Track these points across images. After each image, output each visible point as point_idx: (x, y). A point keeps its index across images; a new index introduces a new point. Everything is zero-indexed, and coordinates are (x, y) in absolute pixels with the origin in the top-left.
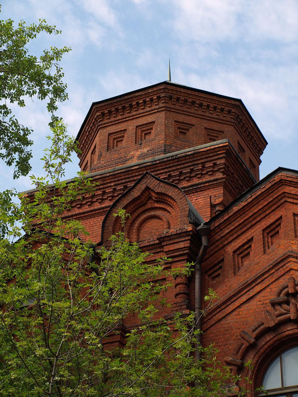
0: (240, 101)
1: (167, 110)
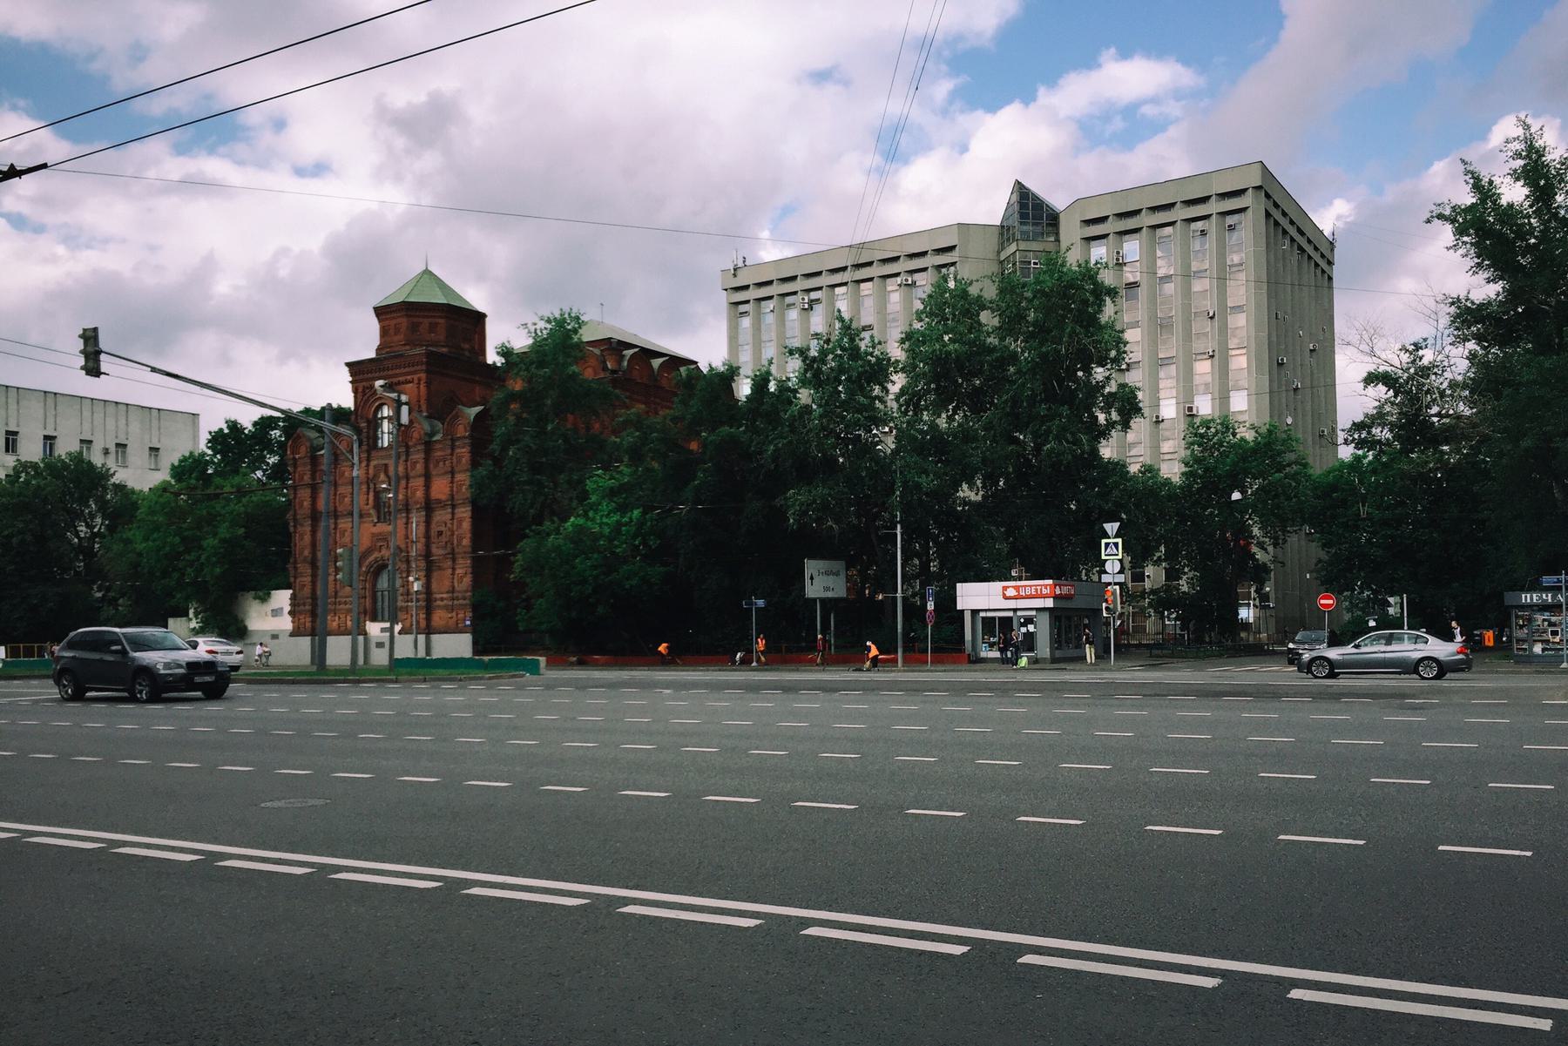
1: (407, 316)
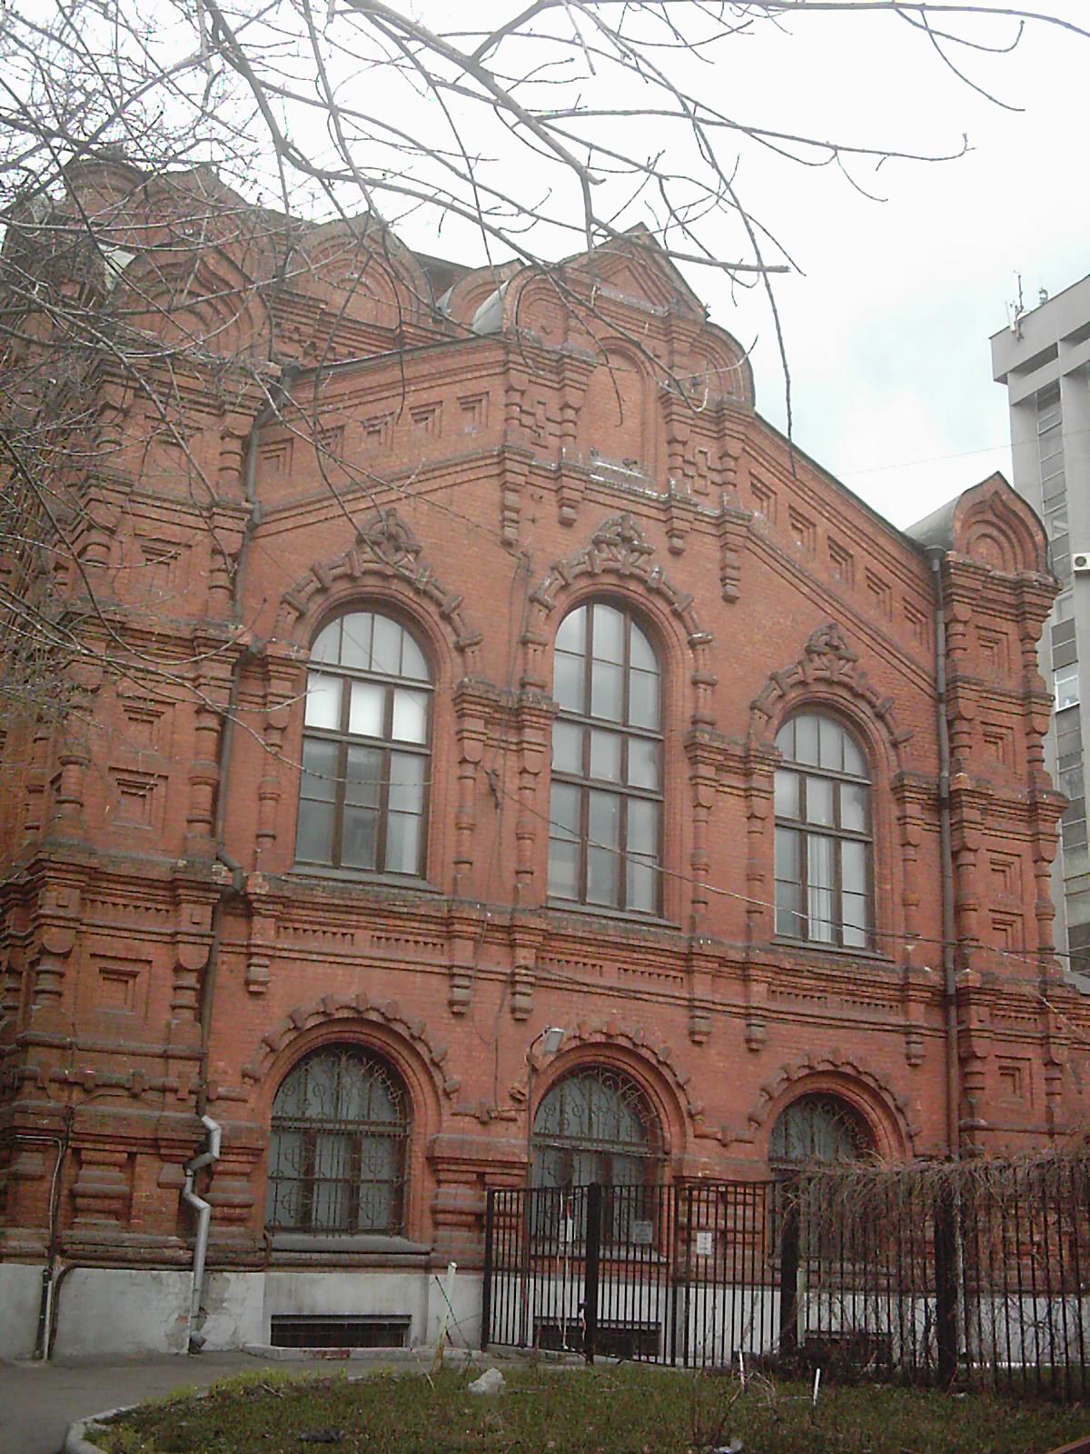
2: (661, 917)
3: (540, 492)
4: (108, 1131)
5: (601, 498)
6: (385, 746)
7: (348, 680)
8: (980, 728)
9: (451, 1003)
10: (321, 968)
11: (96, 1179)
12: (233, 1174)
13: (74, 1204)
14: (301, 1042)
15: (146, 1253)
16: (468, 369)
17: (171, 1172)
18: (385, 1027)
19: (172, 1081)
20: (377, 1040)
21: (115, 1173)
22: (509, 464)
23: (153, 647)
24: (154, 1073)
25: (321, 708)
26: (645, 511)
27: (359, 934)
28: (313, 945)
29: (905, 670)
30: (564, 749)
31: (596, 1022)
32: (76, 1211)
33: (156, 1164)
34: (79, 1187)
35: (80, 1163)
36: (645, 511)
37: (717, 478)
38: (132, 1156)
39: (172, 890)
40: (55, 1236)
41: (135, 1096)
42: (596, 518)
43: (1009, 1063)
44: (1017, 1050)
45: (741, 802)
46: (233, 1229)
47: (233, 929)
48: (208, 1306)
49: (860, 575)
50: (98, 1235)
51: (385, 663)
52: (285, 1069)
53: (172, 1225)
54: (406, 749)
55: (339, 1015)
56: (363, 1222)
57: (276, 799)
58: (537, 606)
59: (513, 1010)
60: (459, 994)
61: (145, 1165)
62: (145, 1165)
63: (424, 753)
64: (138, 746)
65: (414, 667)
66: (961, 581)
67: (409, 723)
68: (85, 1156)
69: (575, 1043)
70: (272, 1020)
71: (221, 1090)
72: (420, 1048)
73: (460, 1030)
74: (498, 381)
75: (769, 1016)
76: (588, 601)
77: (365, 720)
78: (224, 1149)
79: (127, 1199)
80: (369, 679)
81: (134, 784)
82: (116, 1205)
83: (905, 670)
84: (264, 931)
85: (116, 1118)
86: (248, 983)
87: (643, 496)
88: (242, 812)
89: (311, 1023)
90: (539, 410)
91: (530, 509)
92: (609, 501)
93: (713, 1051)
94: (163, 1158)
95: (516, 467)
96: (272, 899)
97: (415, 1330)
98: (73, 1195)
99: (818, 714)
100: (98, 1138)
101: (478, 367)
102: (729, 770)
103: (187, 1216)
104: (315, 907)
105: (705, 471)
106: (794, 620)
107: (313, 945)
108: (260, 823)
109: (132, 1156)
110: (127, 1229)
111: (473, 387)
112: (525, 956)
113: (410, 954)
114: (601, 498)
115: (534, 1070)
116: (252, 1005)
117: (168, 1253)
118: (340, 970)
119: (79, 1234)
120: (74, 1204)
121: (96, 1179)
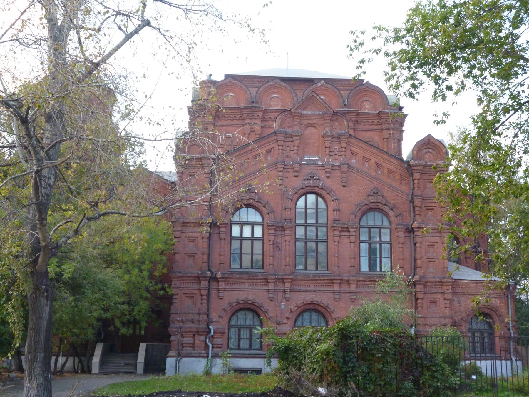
0: (382, 90)
2: (327, 270)
3: (288, 170)
4: (188, 330)
5: (305, 168)
6: (252, 239)
7: (242, 225)
8: (425, 208)
9: (269, 298)
10: (236, 292)
11: (186, 340)
12: (218, 338)
13: (182, 346)
14: (233, 308)
15: (197, 355)
16: (267, 143)
17: (203, 338)
18: (253, 304)
19: (201, 319)
20: (252, 307)
21: (191, 339)
22: (278, 166)
23: (192, 225)
24: (196, 317)
25: (236, 231)
26: (318, 168)
27: (246, 284)
28: (234, 287)
29: (400, 195)
30: (300, 232)
31: (308, 298)
32: (183, 347)
33: (199, 337)
34: (183, 342)
35: (184, 337)
36: (318, 168)
37: (340, 154)
38: (194, 335)
39: (198, 279)
40: (179, 353)
41: (193, 323)
42: (306, 172)
43: (433, 299)
44: (435, 296)
45: (348, 239)
46: (219, 349)
47: (214, 285)
48: (213, 365)
49: (386, 171)
50: (187, 352)
51: (251, 219)
52: (230, 315)
53: (203, 349)
54: (258, 239)
55: (241, 302)
56: (252, 348)
57: (224, 255)
58: (288, 200)
59: (285, 298)
60: (271, 296)
61: (197, 336)
62: (197, 336)
63: (262, 239)
64: (190, 247)
65: (259, 219)
66: (415, 168)
67: (258, 232)
68: (184, 335)
69: (302, 304)
70: (225, 304)
71: (214, 320)
72: (262, 308)
73: (272, 304)
74: (276, 144)
75: (356, 293)
76: (305, 194)
77: (247, 232)
78: (214, 332)
79: (193, 344)
80: (247, 223)
81: (191, 256)
82: (191, 345)
83: (400, 195)
84: (222, 285)
85: (190, 328)
86: (219, 297)
87: (318, 164)
88: (216, 258)
89: (234, 304)
90: (288, 148)
91: (287, 175)
92: (308, 168)
93: (341, 303)
94: (200, 335)
95: (280, 166)
96: (222, 278)
97: (263, 371)
98: (182, 344)
99: (374, 211)
100: (186, 332)
101: (270, 142)
102: (344, 231)
103: (206, 347)
104: (234, 278)
105: (336, 153)
106: (364, 188)
107: (234, 287)
108: (220, 261)
109: (194, 335)
110: (194, 350)
111: (269, 147)
112: (287, 285)
113: (259, 287)
114: (305, 168)
115: (291, 312)
116: (220, 301)
117: (201, 355)
118: (241, 292)
119: (184, 351)
120: (182, 346)
121: (186, 340)
